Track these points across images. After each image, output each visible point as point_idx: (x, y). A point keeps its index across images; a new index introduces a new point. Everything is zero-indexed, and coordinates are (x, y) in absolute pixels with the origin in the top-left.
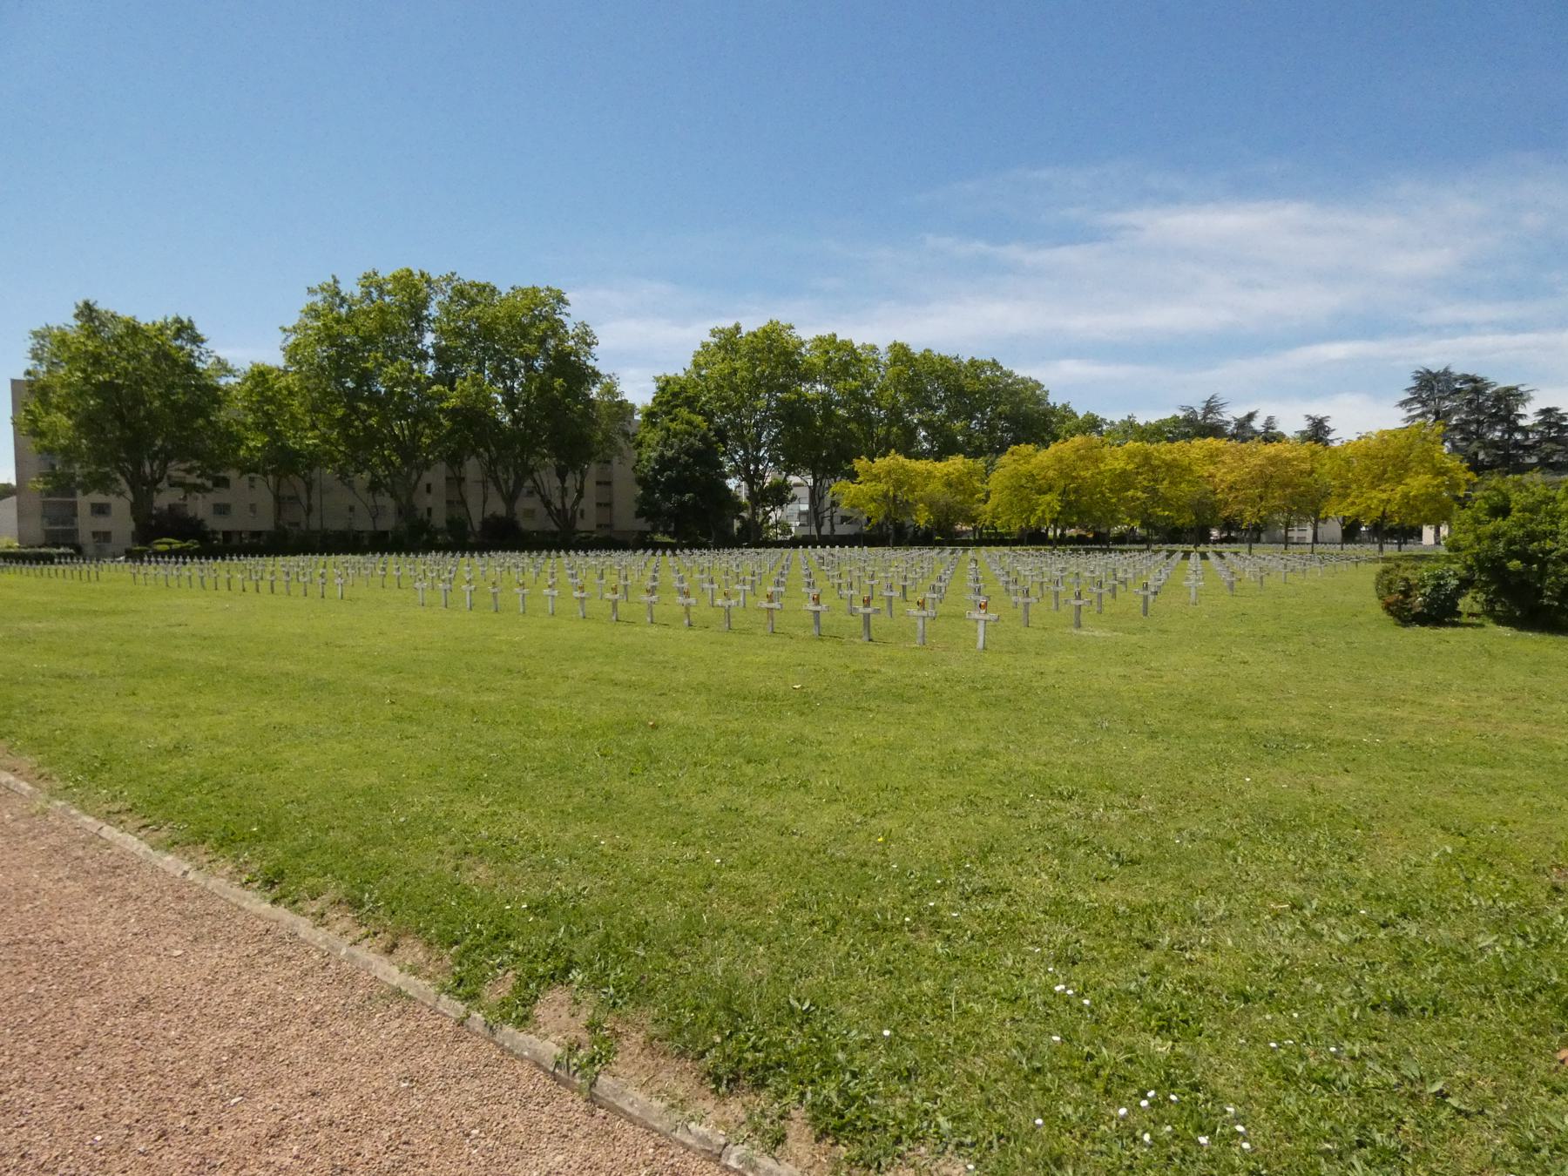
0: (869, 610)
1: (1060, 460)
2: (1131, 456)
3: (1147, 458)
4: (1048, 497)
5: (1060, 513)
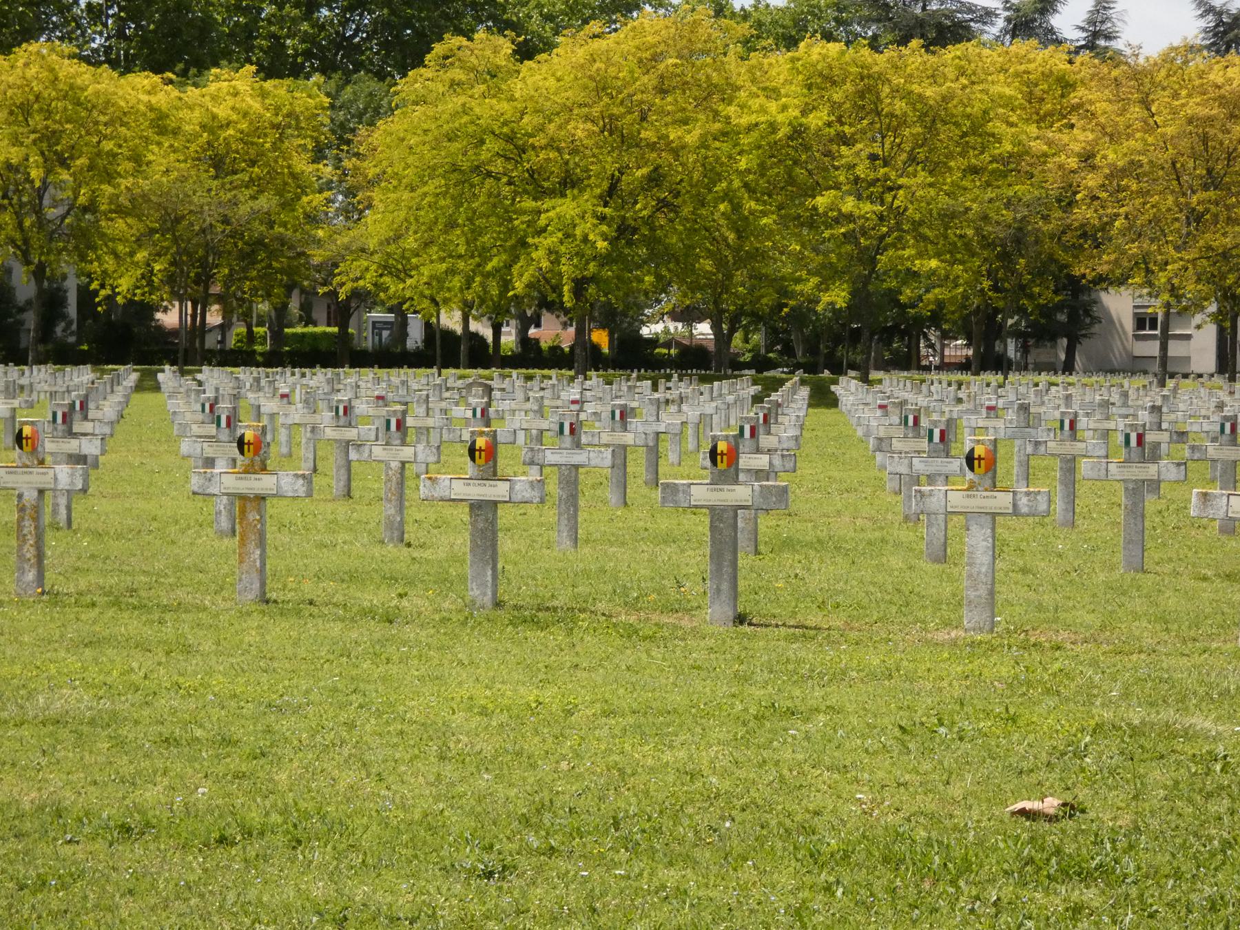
0: (741, 493)
1: (602, 87)
2: (821, 81)
3: (868, 91)
4: (565, 207)
5: (604, 260)
